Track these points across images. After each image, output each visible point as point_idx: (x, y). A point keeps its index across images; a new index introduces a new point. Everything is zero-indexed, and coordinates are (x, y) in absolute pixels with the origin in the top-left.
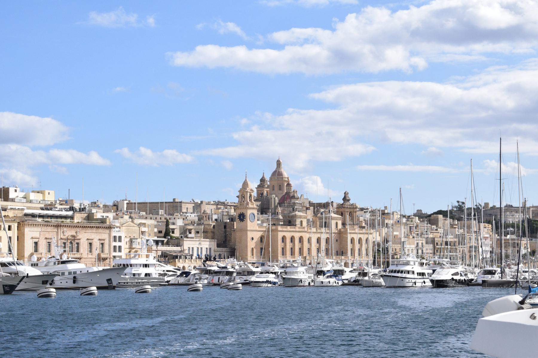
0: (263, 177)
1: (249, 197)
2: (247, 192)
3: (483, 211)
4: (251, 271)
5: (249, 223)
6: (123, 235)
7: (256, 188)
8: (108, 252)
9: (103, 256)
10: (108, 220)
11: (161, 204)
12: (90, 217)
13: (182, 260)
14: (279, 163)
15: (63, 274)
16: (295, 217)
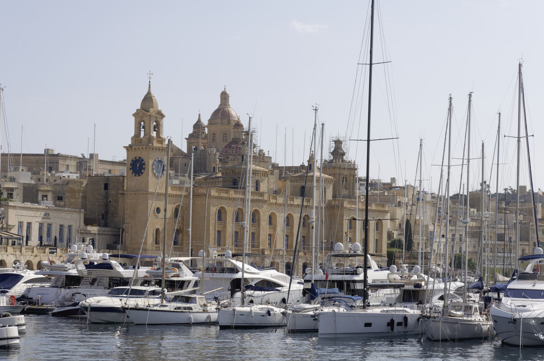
2: (150, 116)
3: (520, 197)
4: (121, 277)
5: (151, 179)
7: (186, 139)
11: (24, 157)
14: (224, 96)
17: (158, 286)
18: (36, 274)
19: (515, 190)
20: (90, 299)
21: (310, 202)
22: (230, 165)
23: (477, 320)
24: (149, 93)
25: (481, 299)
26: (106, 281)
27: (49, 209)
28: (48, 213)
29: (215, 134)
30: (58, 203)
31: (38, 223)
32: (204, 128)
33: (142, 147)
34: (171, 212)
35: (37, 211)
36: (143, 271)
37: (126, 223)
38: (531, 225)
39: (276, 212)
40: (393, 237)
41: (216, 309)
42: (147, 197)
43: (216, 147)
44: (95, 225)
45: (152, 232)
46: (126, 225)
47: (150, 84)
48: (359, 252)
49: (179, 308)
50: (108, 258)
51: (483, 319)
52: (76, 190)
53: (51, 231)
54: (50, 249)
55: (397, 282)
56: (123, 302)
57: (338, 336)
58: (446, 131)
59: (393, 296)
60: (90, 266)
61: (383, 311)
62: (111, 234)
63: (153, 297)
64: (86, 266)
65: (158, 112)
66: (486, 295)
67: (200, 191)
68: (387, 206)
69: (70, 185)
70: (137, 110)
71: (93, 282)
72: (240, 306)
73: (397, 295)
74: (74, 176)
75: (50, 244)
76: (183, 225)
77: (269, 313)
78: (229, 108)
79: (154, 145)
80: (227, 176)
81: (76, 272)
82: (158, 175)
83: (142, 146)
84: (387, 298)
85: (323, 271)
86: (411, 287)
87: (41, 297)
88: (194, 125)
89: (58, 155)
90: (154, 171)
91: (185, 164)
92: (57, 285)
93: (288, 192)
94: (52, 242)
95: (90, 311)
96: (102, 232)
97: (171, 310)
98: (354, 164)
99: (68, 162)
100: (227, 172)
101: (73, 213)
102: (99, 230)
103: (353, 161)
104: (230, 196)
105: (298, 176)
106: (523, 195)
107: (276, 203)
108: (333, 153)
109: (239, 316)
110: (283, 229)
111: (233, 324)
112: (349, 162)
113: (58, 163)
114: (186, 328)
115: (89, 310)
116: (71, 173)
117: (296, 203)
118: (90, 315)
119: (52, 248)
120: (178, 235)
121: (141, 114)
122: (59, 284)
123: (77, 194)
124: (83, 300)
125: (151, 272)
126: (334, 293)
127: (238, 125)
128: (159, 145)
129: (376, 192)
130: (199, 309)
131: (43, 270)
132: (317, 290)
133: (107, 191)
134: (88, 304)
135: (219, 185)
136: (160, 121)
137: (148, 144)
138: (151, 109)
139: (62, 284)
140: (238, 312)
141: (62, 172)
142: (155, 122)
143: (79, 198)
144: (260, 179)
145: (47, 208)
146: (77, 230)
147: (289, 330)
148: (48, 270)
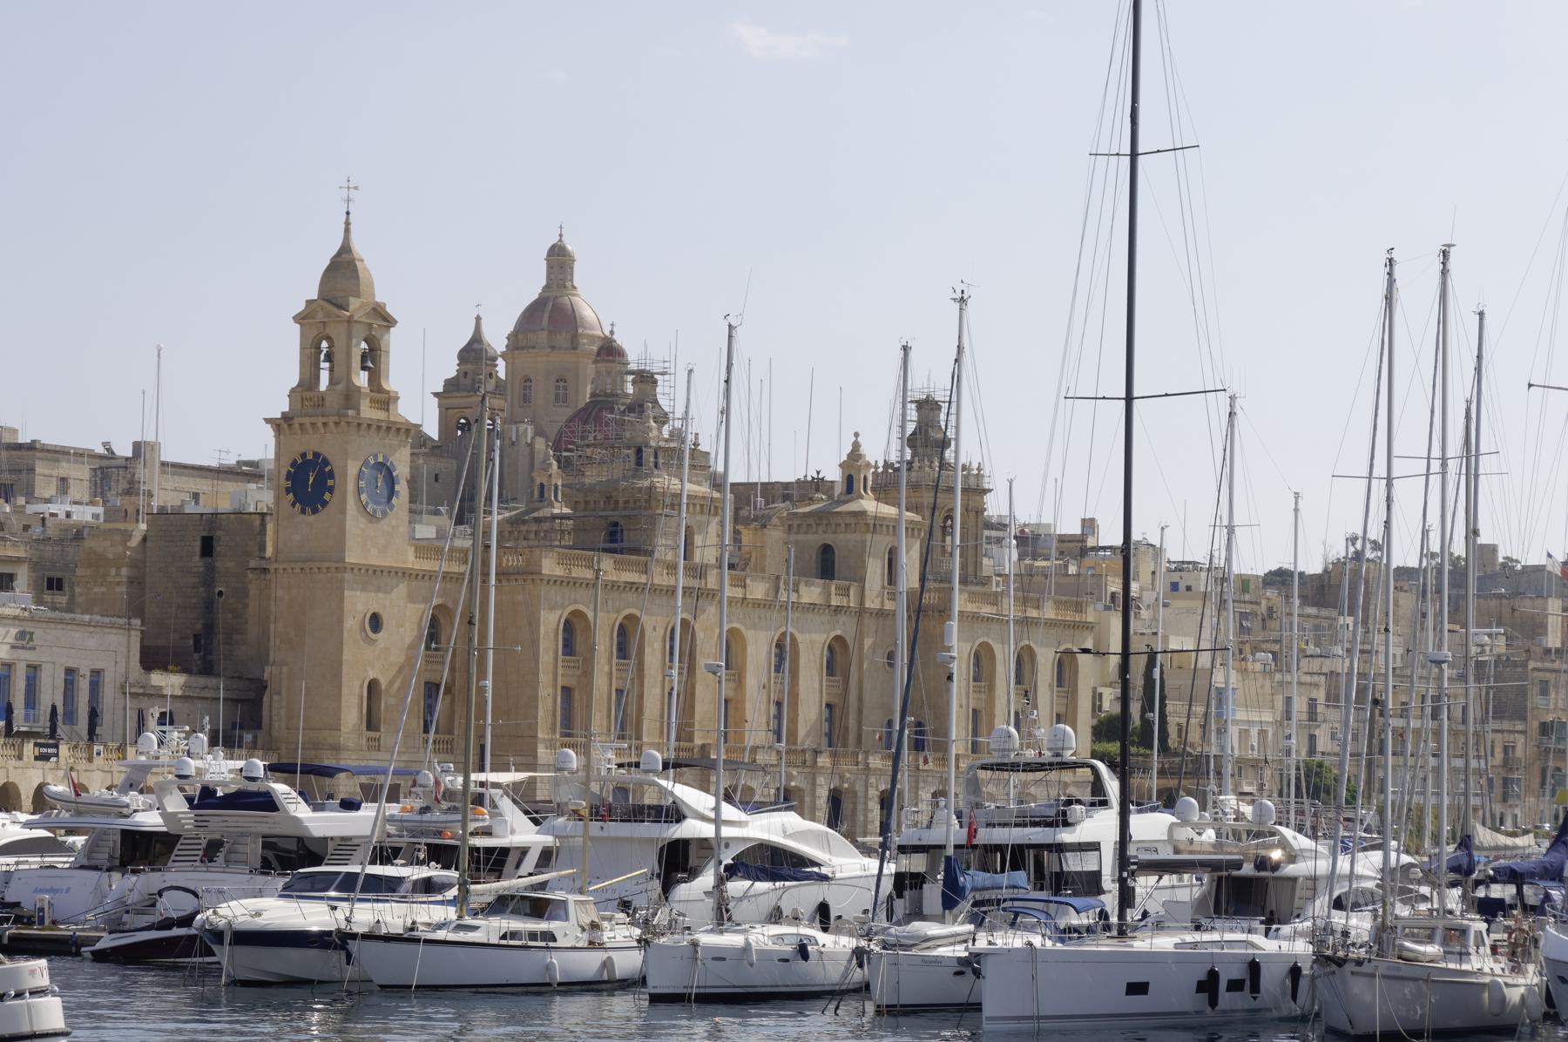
2: (350, 321)
5: (354, 522)
7: (436, 394)
14: (559, 260)
16: (648, 501)
17: (439, 866)
18: (28, 825)
19: (1459, 558)
20: (231, 903)
21: (848, 596)
22: (592, 476)
23: (1487, 970)
24: (346, 249)
25: (1468, 906)
26: (255, 850)
27: (32, 619)
28: (28, 630)
30: (48, 598)
32: (494, 359)
33: (325, 420)
36: (362, 822)
37: (274, 663)
38: (1530, 667)
39: (742, 629)
41: (639, 941)
42: (342, 581)
43: (532, 422)
44: (176, 669)
45: (357, 691)
46: (274, 668)
47: (347, 219)
49: (514, 935)
51: (1503, 969)
52: (110, 556)
53: (37, 688)
54: (36, 745)
55: (1199, 853)
56: (340, 915)
57: (1045, 1025)
58: (1380, 367)
60: (206, 799)
61: (1184, 944)
63: (425, 899)
64: (190, 800)
65: (374, 309)
66: (1481, 893)
67: (508, 560)
68: (1090, 609)
69: (90, 543)
70: (307, 301)
71: (212, 850)
72: (712, 931)
74: (85, 514)
75: (34, 730)
77: (803, 951)
78: (573, 298)
79: (362, 415)
80: (586, 513)
81: (160, 821)
82: (375, 511)
83: (323, 416)
85: (958, 818)
87: (52, 902)
88: (461, 351)
89: (32, 447)
90: (364, 497)
91: (436, 475)
92: (93, 863)
93: (773, 564)
94: (43, 724)
95: (230, 944)
96: (198, 690)
97: (491, 942)
98: (979, 476)
99: (65, 469)
100: (588, 499)
101: (106, 630)
102: (185, 686)
103: (975, 466)
105: (809, 514)
106: (1489, 572)
107: (744, 599)
108: (912, 441)
109: (710, 963)
110: (765, 680)
111: (692, 987)
113: (32, 470)
114: (534, 1002)
115: (227, 939)
116: (76, 503)
117: (805, 600)
118: (232, 957)
119: (42, 741)
121: (320, 315)
122: (102, 857)
123: (113, 571)
124: (208, 908)
125: (401, 821)
126: (1014, 887)
127: (609, 351)
128: (379, 415)
129: (1040, 563)
130: (577, 937)
131: (50, 815)
132: (962, 879)
134: (224, 921)
135: (563, 543)
136: (382, 336)
137: (342, 411)
138: (352, 300)
139: (111, 857)
140: (707, 948)
141: (48, 501)
142: (365, 340)
143: (118, 584)
145: (26, 614)
146: (118, 684)
147: (879, 1006)
148: (65, 815)
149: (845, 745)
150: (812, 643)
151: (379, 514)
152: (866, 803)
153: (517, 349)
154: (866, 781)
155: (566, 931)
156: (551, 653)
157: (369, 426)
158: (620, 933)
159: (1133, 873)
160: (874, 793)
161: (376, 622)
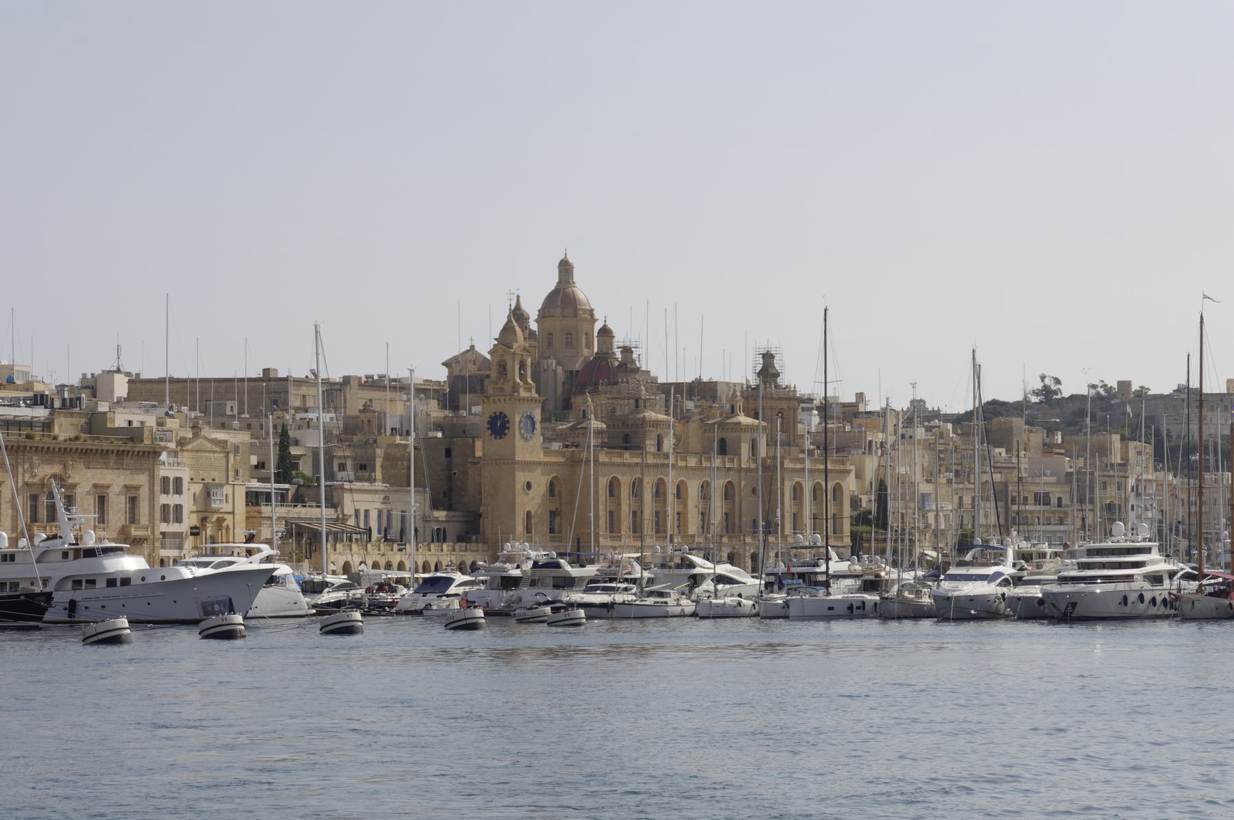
0: (518, 307)
1: (520, 370)
2: (514, 354)
4: (566, 575)
5: (519, 442)
6: (185, 474)
8: (147, 523)
9: (135, 532)
10: (146, 434)
12: (95, 424)
13: (343, 546)
14: (565, 268)
15: (92, 582)
21: (734, 462)
26: (551, 582)
29: (552, 334)
30: (360, 474)
31: (376, 511)
34: (545, 487)
35: (375, 494)
40: (861, 505)
42: (514, 468)
45: (522, 516)
48: (819, 544)
49: (658, 602)
50: (555, 556)
52: (398, 456)
54: (398, 545)
59: (854, 587)
62: (458, 521)
73: (857, 587)
76: (561, 504)
84: (849, 588)
86: (871, 577)
89: (285, 380)
90: (522, 431)
103: (792, 386)
104: (625, 461)
108: (759, 374)
112: (787, 387)
120: (554, 519)
122: (495, 586)
123: (400, 463)
133: (449, 458)
138: (514, 344)
139: (498, 586)
140: (715, 604)
144: (662, 433)
145: (387, 489)
149: (734, 532)
150: (718, 484)
151: (529, 438)
152: (745, 559)
153: (544, 317)
154: (745, 548)
155: (671, 601)
156: (604, 496)
157: (524, 400)
158: (685, 602)
159: (830, 578)
160: (748, 554)
161: (529, 486)
